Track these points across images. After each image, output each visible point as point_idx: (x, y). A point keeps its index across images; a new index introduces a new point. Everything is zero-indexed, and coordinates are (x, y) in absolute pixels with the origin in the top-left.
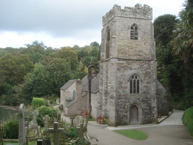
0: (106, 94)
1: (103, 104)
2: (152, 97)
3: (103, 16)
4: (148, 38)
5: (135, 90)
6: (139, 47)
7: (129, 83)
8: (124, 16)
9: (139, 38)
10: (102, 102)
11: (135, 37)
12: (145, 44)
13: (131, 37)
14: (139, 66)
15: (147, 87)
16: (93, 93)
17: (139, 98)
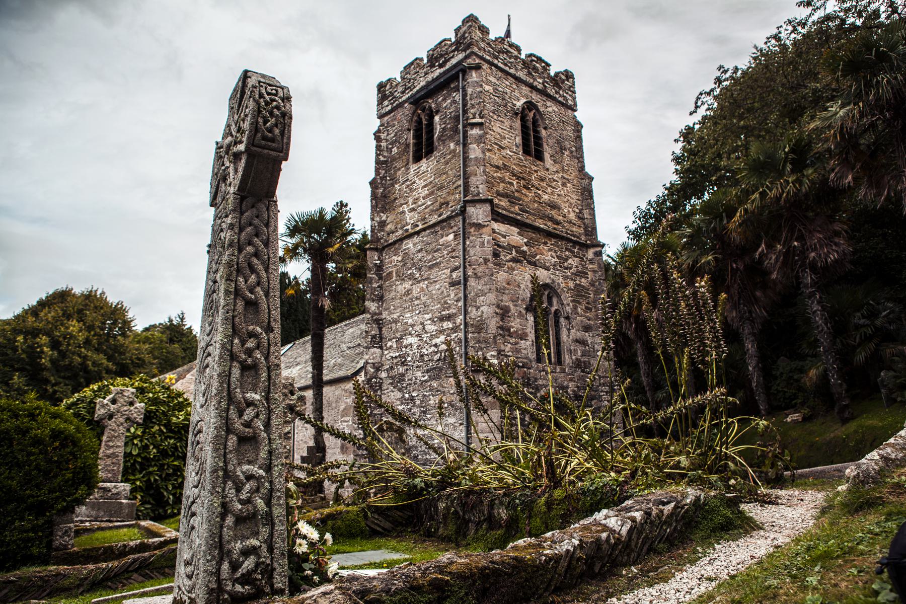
2: (604, 385)
8: (500, 65)
14: (556, 259)
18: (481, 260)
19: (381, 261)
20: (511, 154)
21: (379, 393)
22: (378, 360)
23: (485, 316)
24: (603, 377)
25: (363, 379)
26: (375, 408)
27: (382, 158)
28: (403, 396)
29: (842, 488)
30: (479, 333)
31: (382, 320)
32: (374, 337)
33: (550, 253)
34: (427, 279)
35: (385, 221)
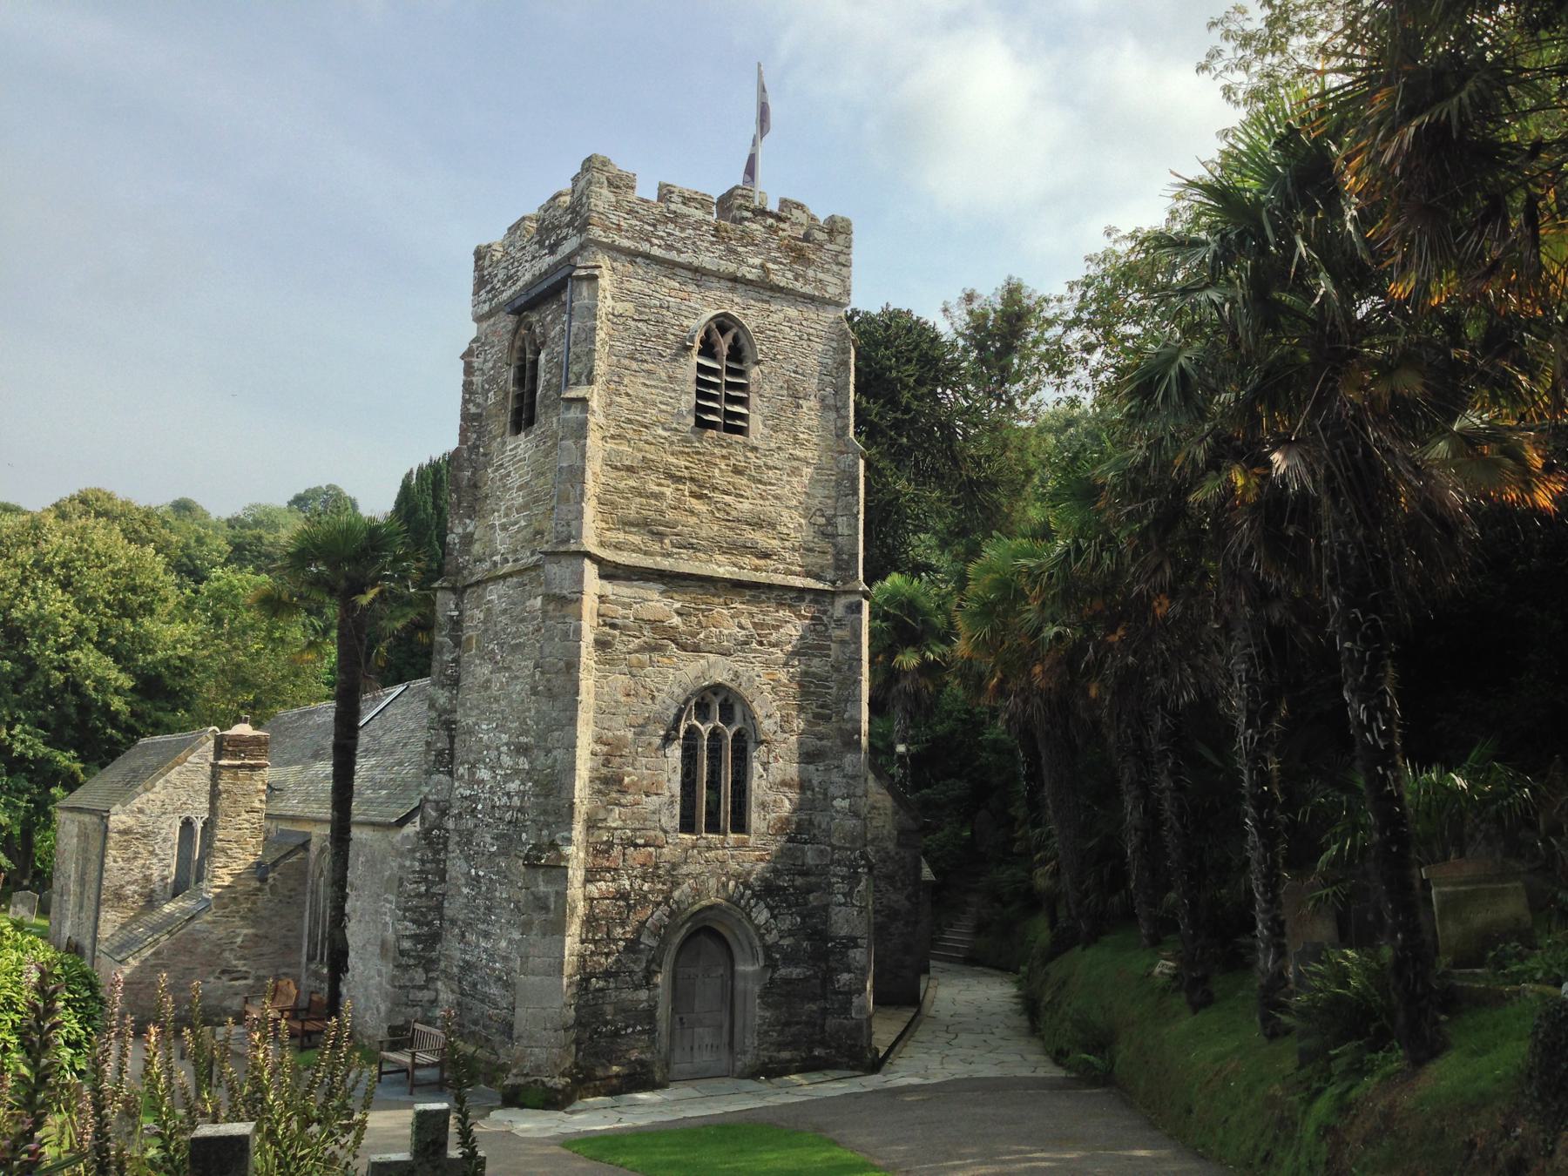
2: (839, 863)
7: (675, 752)
8: (656, 251)
9: (756, 424)
10: (439, 908)
13: (699, 408)
18: (562, 664)
20: (666, 434)
21: (442, 856)
22: (444, 795)
23: (558, 767)
24: (840, 848)
25: (418, 829)
26: (434, 883)
27: (473, 410)
28: (469, 872)
30: (547, 796)
31: (455, 722)
32: (440, 753)
34: (508, 669)
35: (472, 534)
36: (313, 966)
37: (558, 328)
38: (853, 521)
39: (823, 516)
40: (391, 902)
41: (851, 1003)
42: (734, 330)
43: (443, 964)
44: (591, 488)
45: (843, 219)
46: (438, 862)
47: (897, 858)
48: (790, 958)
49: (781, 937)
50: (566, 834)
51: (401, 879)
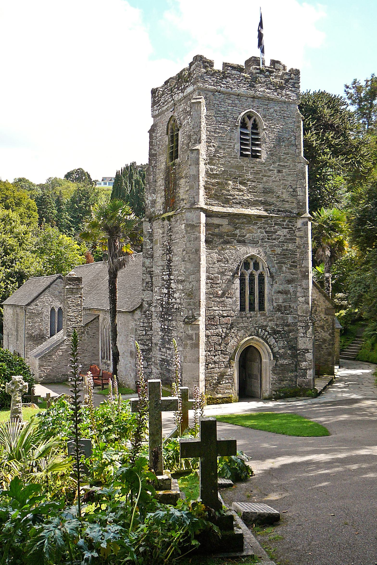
0: (166, 314)
1: (156, 344)
2: (301, 321)
3: (155, 87)
4: (288, 154)
5: (252, 302)
6: (265, 179)
10: (151, 339)
11: (253, 151)
12: (279, 171)
13: (242, 149)
14: (265, 234)
15: (286, 292)
16: (120, 312)
17: (265, 324)
19: (152, 230)
21: (150, 321)
24: (301, 316)
29: (27, 501)
31: (153, 271)
32: (147, 283)
33: (259, 230)
36: (104, 361)
37: (186, 121)
38: (303, 190)
39: (292, 188)
40: (133, 338)
41: (306, 373)
42: (254, 117)
43: (153, 360)
44: (202, 183)
45: (296, 70)
46: (149, 323)
47: (325, 319)
48: (283, 356)
49: (279, 349)
50: (198, 313)
51: (136, 329)
